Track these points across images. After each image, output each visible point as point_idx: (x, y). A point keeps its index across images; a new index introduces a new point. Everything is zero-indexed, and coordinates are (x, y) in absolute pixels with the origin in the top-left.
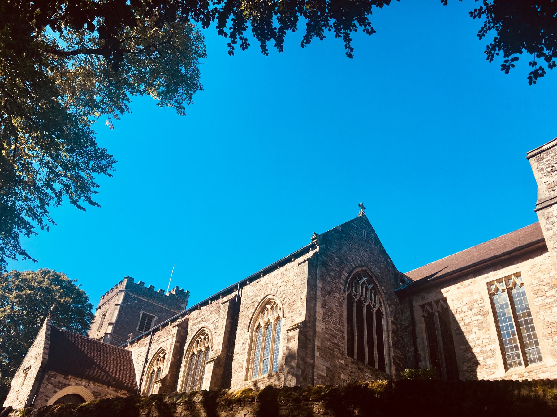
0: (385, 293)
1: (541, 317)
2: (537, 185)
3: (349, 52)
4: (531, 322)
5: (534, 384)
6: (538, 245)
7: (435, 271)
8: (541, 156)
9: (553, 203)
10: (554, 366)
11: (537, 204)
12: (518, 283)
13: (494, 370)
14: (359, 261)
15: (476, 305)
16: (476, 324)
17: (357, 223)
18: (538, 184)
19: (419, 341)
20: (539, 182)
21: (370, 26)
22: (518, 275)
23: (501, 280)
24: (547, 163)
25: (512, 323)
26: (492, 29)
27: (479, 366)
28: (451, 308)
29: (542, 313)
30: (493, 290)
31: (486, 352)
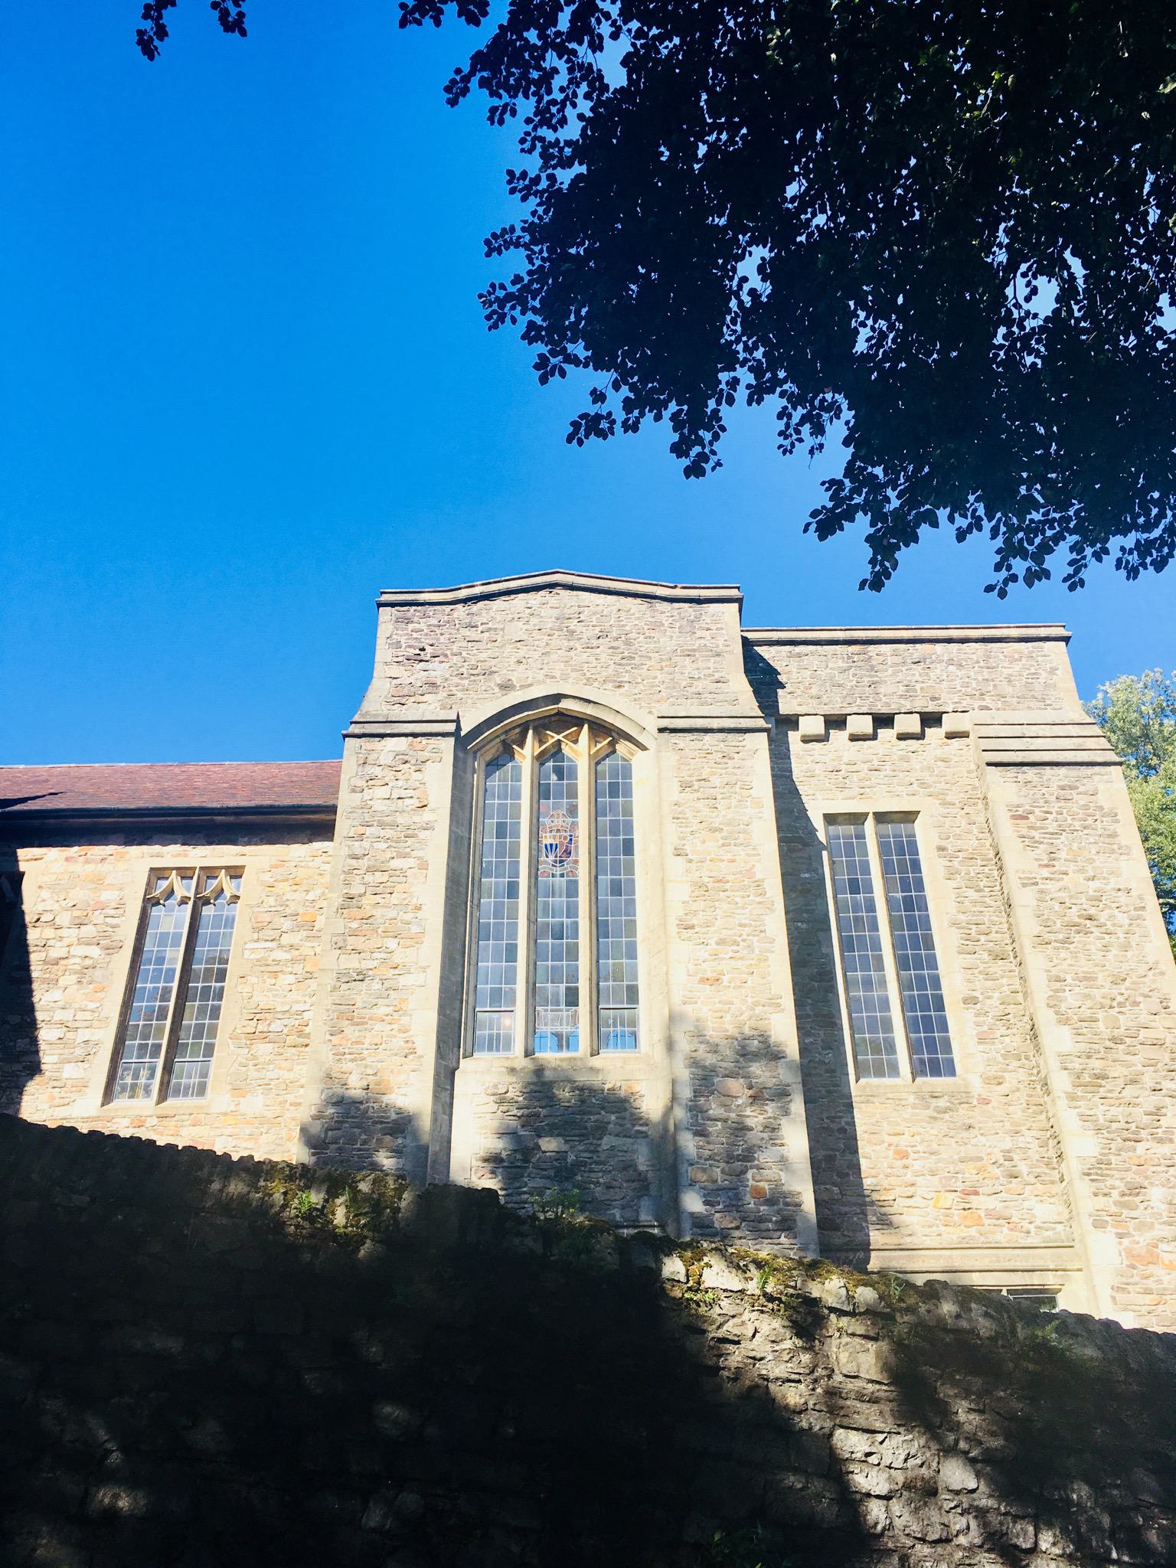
1: (247, 989)
2: (372, 678)
3: (151, 34)
4: (219, 995)
5: (268, 1172)
6: (311, 817)
7: (20, 791)
8: (409, 615)
9: (388, 732)
10: (225, 1114)
11: (354, 720)
12: (227, 894)
13: (73, 1096)
15: (98, 917)
16: (77, 967)
18: (375, 674)
20: (379, 670)
21: (239, 6)
22: (235, 873)
23: (189, 873)
24: (415, 635)
25: (171, 987)
26: (522, 249)
27: (37, 1079)
28: (26, 907)
29: (254, 980)
30: (158, 892)
31: (72, 1046)
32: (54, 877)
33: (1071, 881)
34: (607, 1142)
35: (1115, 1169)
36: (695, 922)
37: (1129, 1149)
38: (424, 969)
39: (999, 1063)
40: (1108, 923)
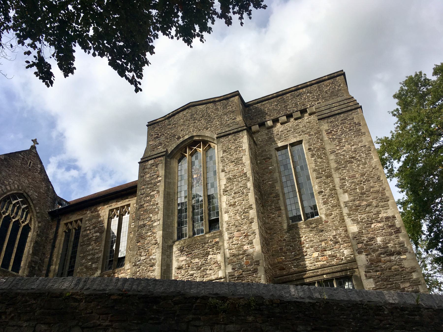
0: (37, 213)
8: (155, 126)
14: (16, 186)
17: (24, 154)
19: (56, 250)
24: (156, 131)
32: (89, 218)
33: (347, 147)
34: (210, 257)
35: (365, 234)
36: (228, 189)
37: (368, 227)
38: (159, 220)
39: (330, 209)
40: (359, 158)
